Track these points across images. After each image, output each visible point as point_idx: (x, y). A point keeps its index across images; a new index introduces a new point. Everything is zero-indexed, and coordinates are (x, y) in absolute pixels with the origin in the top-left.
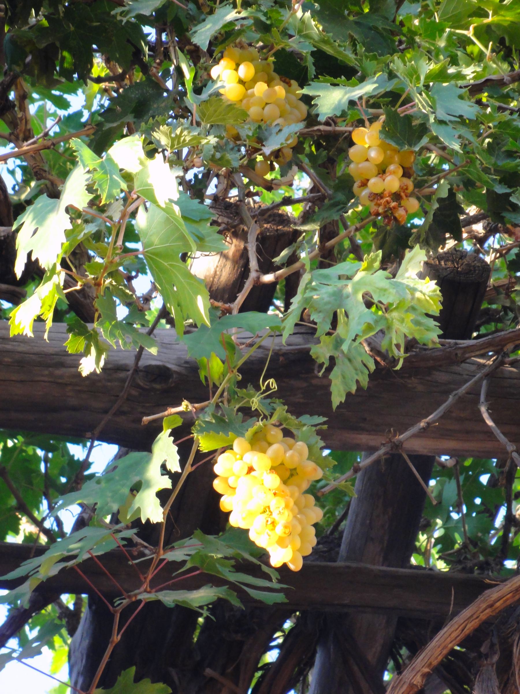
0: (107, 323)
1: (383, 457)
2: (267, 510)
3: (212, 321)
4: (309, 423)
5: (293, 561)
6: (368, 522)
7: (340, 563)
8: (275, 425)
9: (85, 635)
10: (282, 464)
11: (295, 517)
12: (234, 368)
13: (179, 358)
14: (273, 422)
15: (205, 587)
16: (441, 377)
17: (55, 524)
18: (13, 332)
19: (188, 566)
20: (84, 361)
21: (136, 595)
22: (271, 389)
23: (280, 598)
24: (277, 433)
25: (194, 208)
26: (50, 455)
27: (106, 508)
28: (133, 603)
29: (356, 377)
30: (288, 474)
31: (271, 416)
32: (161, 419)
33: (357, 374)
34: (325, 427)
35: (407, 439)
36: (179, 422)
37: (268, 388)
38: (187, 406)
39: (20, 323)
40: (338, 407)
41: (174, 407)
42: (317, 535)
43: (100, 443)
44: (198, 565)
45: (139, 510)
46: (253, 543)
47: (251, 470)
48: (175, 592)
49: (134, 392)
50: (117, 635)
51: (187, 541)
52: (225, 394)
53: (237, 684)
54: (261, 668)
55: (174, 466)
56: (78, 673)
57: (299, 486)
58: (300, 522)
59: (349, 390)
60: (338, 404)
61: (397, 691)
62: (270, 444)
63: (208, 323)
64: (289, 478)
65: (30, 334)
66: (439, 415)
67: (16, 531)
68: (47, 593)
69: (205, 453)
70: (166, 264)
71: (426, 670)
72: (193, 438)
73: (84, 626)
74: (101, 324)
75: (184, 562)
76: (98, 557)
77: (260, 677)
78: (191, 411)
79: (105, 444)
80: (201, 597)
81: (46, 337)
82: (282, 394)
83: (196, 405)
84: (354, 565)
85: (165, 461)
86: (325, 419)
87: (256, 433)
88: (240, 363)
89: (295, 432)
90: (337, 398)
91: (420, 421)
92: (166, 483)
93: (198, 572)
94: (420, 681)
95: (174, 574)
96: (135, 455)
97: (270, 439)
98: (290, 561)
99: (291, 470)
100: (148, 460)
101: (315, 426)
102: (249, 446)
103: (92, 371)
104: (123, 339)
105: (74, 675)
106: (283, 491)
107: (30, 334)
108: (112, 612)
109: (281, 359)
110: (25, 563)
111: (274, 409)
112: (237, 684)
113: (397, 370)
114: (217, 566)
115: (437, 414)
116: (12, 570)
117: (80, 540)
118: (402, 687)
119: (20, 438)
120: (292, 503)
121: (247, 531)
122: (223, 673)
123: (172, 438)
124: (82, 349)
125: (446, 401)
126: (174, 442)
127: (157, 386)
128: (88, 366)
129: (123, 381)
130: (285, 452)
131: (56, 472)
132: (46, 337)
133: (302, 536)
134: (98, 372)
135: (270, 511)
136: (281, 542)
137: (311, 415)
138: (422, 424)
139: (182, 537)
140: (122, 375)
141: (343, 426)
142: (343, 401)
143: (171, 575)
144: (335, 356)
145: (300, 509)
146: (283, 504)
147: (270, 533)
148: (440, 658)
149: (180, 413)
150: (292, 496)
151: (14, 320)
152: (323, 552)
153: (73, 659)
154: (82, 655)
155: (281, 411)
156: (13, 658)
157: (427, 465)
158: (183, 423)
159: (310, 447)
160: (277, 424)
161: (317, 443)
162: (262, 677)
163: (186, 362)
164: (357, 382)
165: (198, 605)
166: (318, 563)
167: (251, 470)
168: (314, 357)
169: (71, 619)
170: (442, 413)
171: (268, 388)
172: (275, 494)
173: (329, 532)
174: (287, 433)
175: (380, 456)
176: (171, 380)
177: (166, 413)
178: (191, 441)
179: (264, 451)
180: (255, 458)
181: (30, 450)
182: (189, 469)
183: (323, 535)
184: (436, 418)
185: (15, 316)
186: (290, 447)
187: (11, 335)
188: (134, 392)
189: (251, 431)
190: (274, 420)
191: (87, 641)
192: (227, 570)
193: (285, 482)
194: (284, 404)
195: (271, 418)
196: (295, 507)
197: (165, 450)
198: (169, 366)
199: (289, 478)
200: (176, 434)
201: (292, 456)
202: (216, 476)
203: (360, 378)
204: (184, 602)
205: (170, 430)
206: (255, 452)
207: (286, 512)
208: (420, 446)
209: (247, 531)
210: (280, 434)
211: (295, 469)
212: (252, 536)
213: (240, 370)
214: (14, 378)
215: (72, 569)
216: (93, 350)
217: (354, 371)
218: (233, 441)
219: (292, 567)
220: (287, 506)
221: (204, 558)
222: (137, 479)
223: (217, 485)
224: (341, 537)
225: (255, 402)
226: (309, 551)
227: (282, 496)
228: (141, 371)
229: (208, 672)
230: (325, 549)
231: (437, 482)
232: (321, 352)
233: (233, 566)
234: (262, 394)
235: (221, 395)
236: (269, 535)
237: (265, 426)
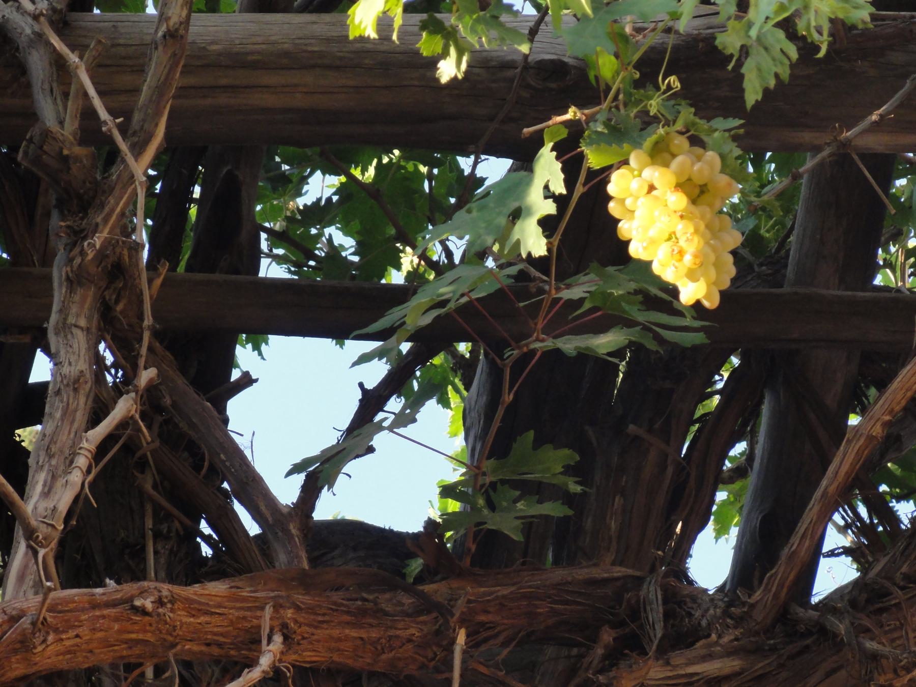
0: (467, 18)
1: (828, 160)
2: (672, 237)
3: (595, 9)
4: (723, 127)
5: (707, 297)
6: (818, 236)
7: (786, 289)
8: (681, 133)
9: (482, 390)
10: (689, 180)
11: (707, 243)
12: (629, 64)
14: (679, 129)
15: (614, 330)
16: (897, 57)
17: (443, 255)
18: (353, 34)
19: (587, 305)
20: (442, 65)
21: (527, 345)
22: (672, 89)
23: (699, 338)
24: (681, 142)
26: (436, 171)
27: (479, 242)
28: (525, 354)
29: (775, 69)
30: (697, 191)
31: (674, 122)
32: (541, 131)
33: (776, 66)
34: (742, 131)
35: (856, 136)
36: (564, 134)
37: (669, 88)
38: (575, 113)
39: (361, 22)
40: (754, 107)
41: (559, 115)
42: (735, 263)
43: (487, 157)
44: (598, 304)
45: (518, 243)
46: (658, 278)
47: (652, 188)
48: (578, 337)
49: (525, 94)
50: (509, 394)
51: (582, 278)
52: (621, 96)
53: (667, 442)
54: (698, 420)
55: (559, 188)
56: (476, 437)
57: (711, 206)
58: (714, 250)
59: (766, 85)
60: (753, 102)
61: (853, 445)
62: (674, 156)
63: (589, 10)
65: (373, 35)
66: (896, 104)
67: (398, 267)
68: (430, 341)
69: (598, 170)
71: (887, 418)
72: (582, 152)
73: (480, 380)
74: (460, 18)
75: (581, 301)
76: (478, 299)
77: (698, 431)
78: (579, 120)
79: (492, 159)
80: (605, 342)
81: (395, 37)
82: (688, 94)
83: (586, 111)
84: (802, 290)
85: (548, 181)
86: (742, 122)
87: (657, 143)
88: (636, 57)
89: (705, 138)
90: (752, 96)
91: (871, 113)
92: (550, 208)
93: (599, 314)
94: (880, 431)
95: (570, 317)
96: (523, 173)
97: (673, 149)
98: (705, 297)
99: (700, 186)
100: (528, 182)
101: (729, 130)
102: (648, 160)
103: (453, 76)
104: (487, 37)
105: (471, 439)
106: (691, 213)
107: (373, 35)
108: (500, 366)
109: (701, 45)
110: (390, 311)
111: (679, 112)
112: (667, 442)
113: (819, 59)
114: (623, 304)
115: (891, 105)
116: (375, 321)
117: (450, 284)
118: (859, 440)
119: (397, 152)
120: (702, 226)
121: (649, 263)
122: (650, 431)
123: (555, 153)
124: (439, 50)
125: (902, 87)
126: (557, 158)
127: (553, 85)
128: (449, 69)
129: (511, 80)
130: (693, 164)
131: (443, 191)
132: (395, 37)
133: (717, 265)
134: (460, 77)
135: (677, 238)
136: (692, 275)
137: (725, 117)
138: (874, 117)
139: (577, 272)
140: (509, 73)
141: (767, 127)
143: (568, 318)
144: (749, 44)
145: (712, 232)
146: (691, 230)
147: (677, 264)
148: (903, 403)
149: (566, 124)
150: (702, 218)
151: (354, 18)
152: (767, 275)
153: (468, 420)
154: (479, 416)
155: (687, 114)
156: (383, 429)
157: (885, 166)
158: (569, 134)
159: (723, 157)
160: (684, 130)
161: (731, 151)
162: (698, 430)
164: (777, 76)
165: (605, 351)
166: (760, 290)
167: (652, 188)
168: (720, 47)
169: (466, 368)
170: (898, 102)
171: (669, 88)
172: (682, 217)
173: (773, 251)
174: (695, 141)
175: (824, 159)
177: (550, 122)
178: (581, 157)
179: (666, 165)
180: (653, 174)
181: (410, 167)
182: (579, 190)
183: (767, 254)
184: (891, 109)
185: (354, 13)
186: (699, 159)
187: (351, 37)
188: (525, 94)
189: (649, 142)
190: (679, 126)
191: (485, 398)
192: (636, 308)
193: (694, 201)
194: (691, 105)
195: (674, 124)
196: (707, 231)
197: (548, 170)
198: (566, 60)
199: (699, 196)
200: (560, 149)
201: (700, 170)
202: (609, 198)
203: (779, 70)
204: (587, 348)
205: (551, 144)
206: (656, 167)
207: (696, 239)
208: (877, 143)
209: (649, 263)
210: (686, 144)
211: (705, 185)
212: (656, 269)
213: (637, 66)
214: (377, 84)
215: (447, 315)
216: (452, 51)
217: (771, 62)
218: (629, 154)
219: (706, 304)
220: (696, 231)
221: (607, 296)
222: (515, 205)
223: (613, 208)
224: (787, 256)
225: (654, 105)
226: (726, 284)
227: (690, 219)
228: (531, 68)
229: (632, 428)
230: (770, 271)
231: (908, 180)
232: (729, 41)
233: (641, 303)
234: (664, 93)
235: (616, 98)
236: (676, 268)
237: (667, 134)
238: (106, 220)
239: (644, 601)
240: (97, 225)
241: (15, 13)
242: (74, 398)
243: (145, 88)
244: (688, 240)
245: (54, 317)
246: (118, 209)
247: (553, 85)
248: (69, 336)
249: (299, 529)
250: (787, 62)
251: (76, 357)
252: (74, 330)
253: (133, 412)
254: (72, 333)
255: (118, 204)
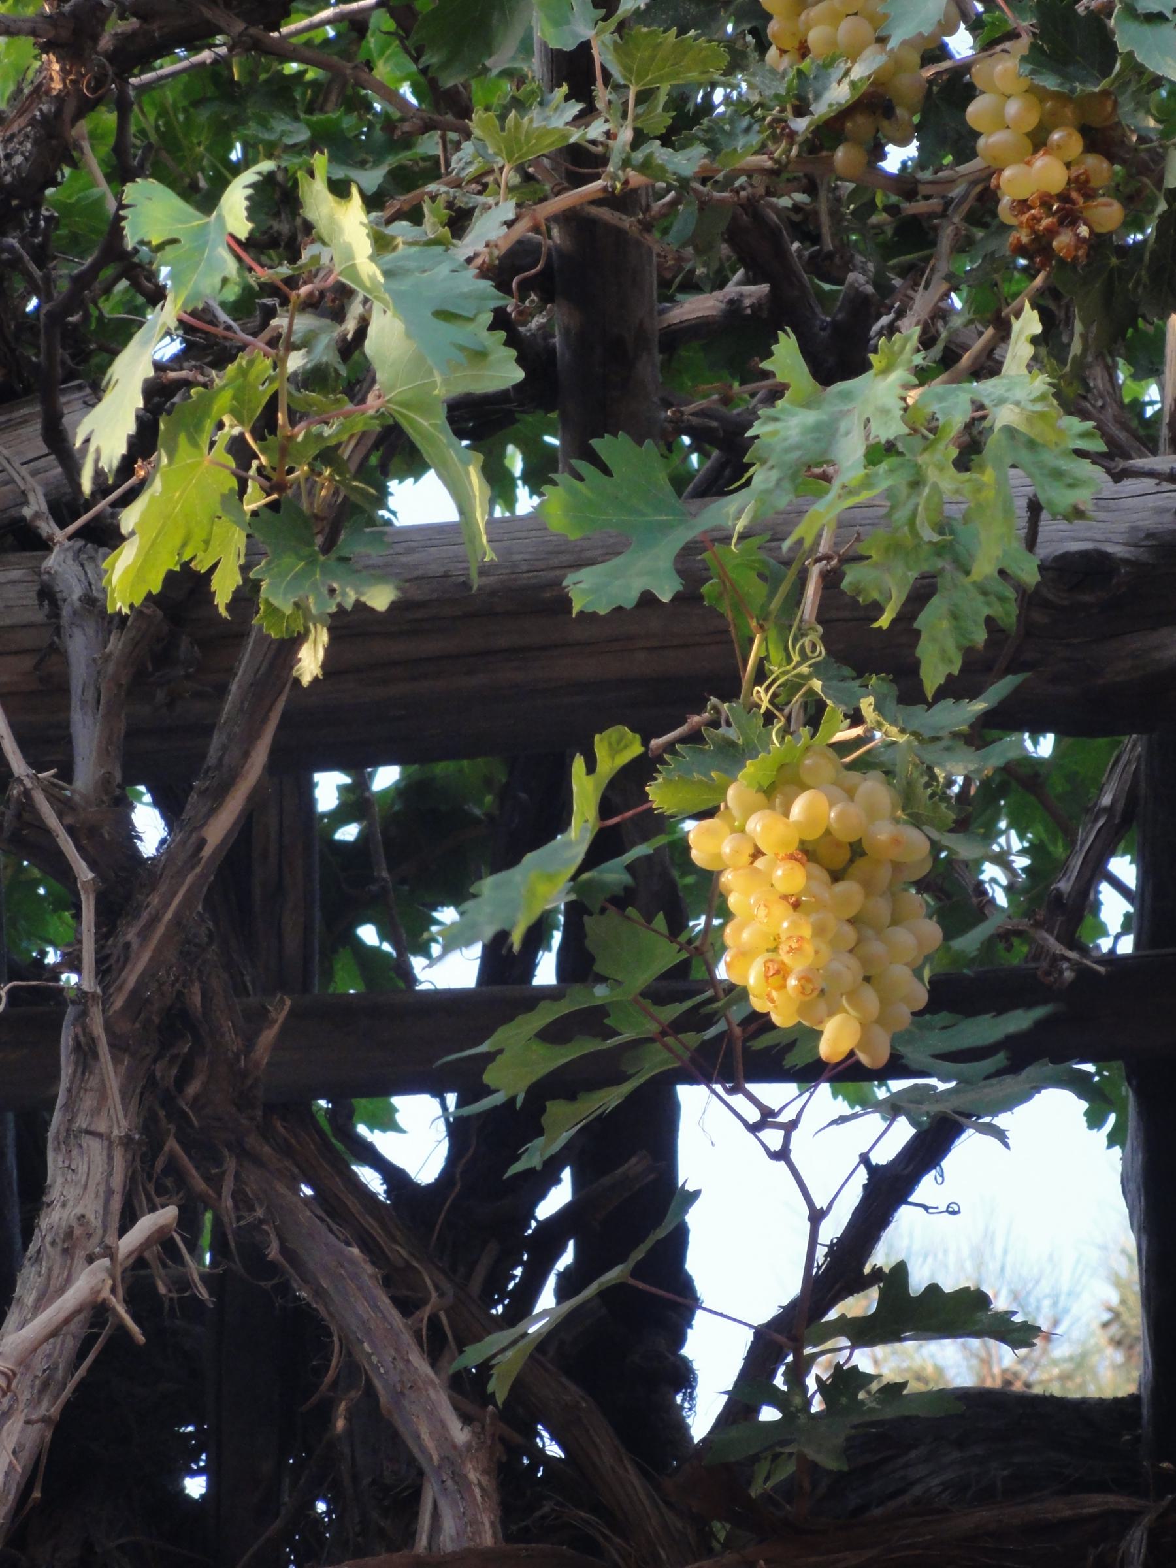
5: (865, 1042)
13: (1134, 529)
25: (466, 290)
29: (986, 611)
33: (989, 604)
59: (967, 644)
64: (852, 861)
70: (426, 424)
127: (1087, 598)
142: (956, 672)
163: (1150, 535)
167: (757, 853)
176: (1114, 581)
191: (1140, 1157)
203: (996, 610)
238: (144, 934)
239: (1122, 1559)
240: (127, 946)
241: (70, 562)
242: (63, 1267)
243: (234, 687)
244: (791, 949)
245: (57, 1119)
246: (169, 915)
247: (1087, 598)
248: (75, 1152)
249: (484, 1472)
250: (1011, 594)
251: (79, 1191)
252: (87, 1141)
253: (106, 1293)
254: (80, 1146)
255: (167, 905)
